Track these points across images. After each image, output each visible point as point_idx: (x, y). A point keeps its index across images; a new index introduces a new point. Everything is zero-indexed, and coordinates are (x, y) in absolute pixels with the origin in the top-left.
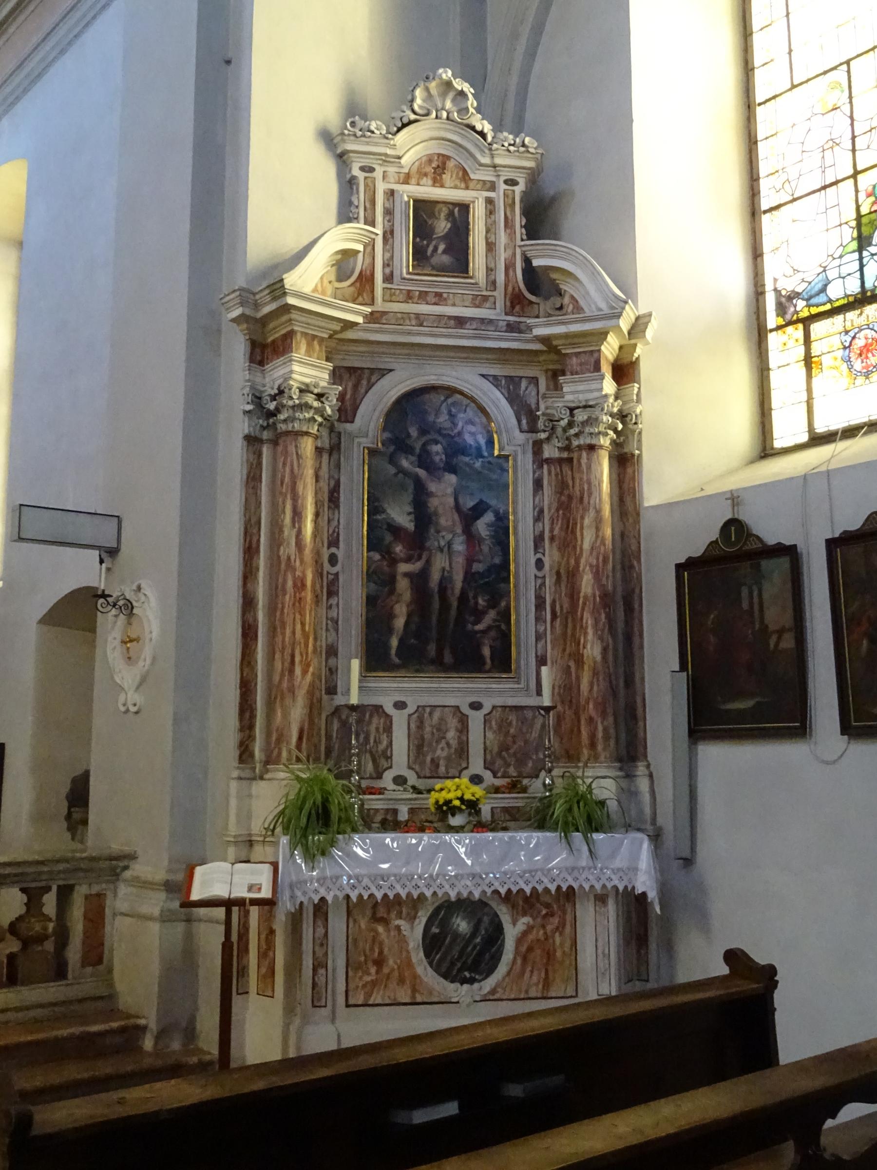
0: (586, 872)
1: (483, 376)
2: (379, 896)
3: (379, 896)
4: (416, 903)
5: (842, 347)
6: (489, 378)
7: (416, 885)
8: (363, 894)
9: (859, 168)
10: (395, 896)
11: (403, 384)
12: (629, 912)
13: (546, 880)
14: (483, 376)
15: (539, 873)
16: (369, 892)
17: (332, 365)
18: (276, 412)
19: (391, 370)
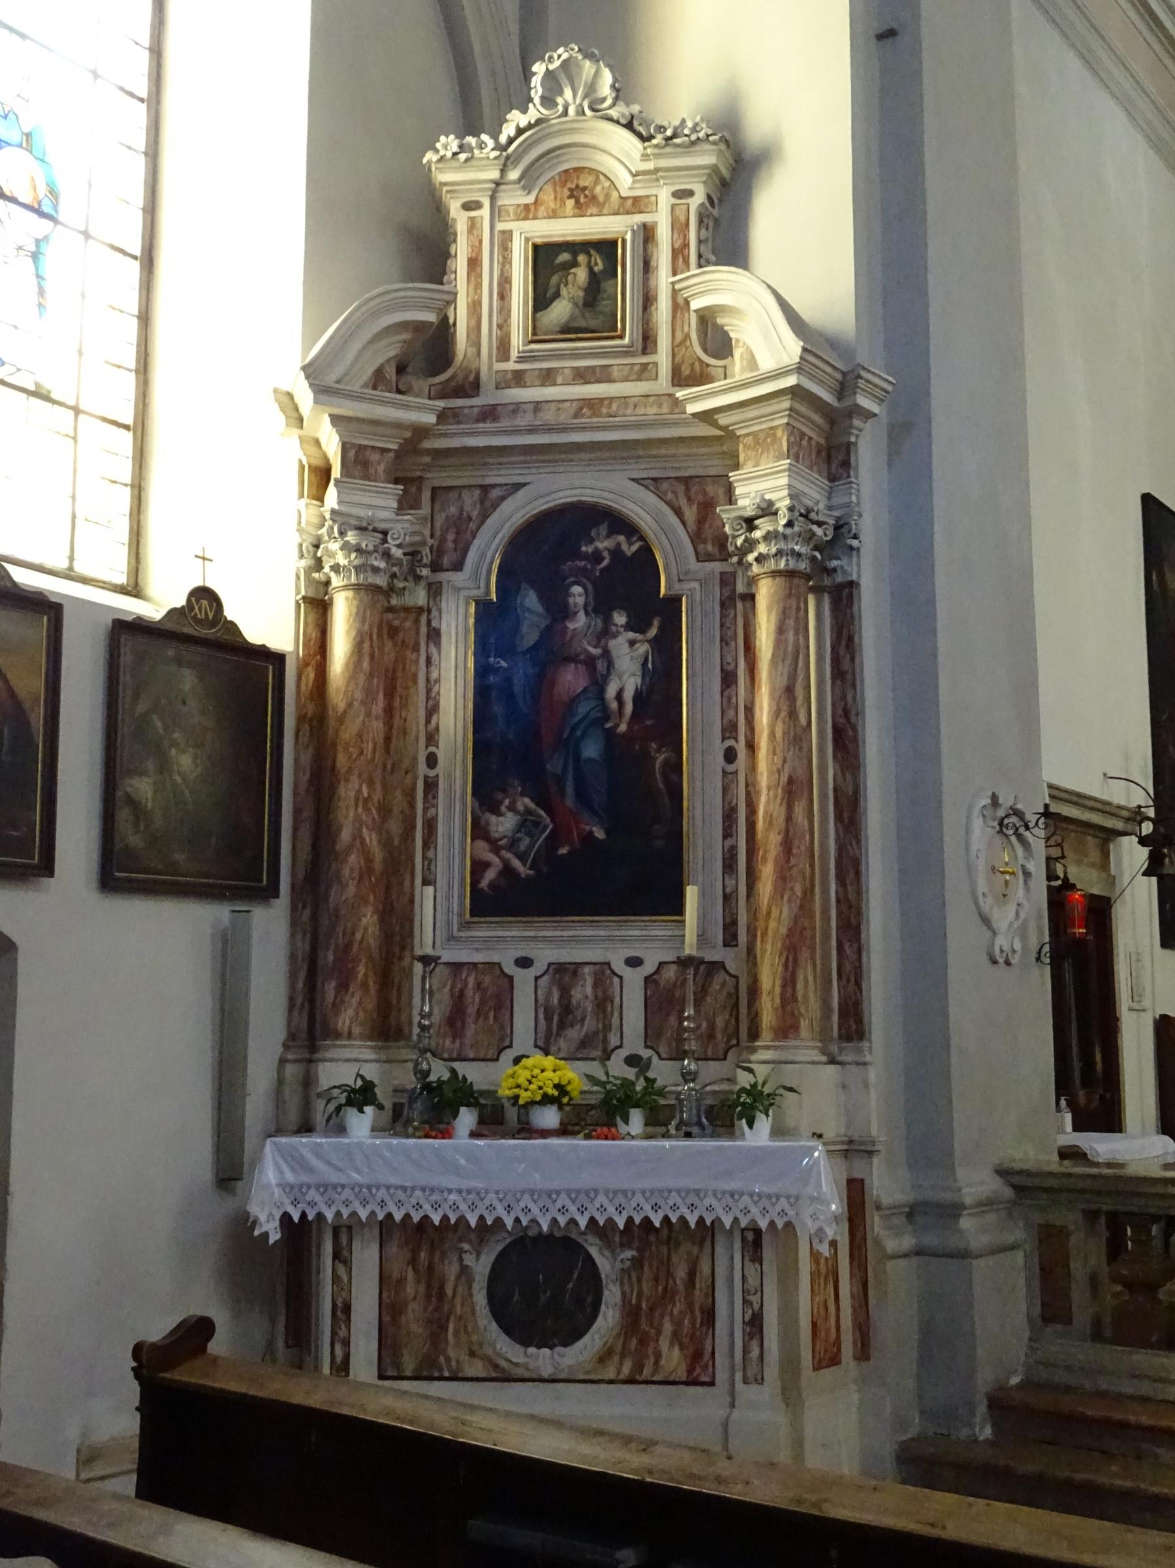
0: (383, 1191)
1: (633, 480)
2: (398, 1216)
3: (398, 1216)
4: (486, 1230)
5: (81, 417)
6: (645, 482)
7: (418, 1204)
8: (705, 1217)
9: (82, 229)
10: (678, 1219)
11: (544, 500)
12: (318, 1273)
13: (573, 1209)
14: (633, 480)
15: (563, 1195)
16: (786, 1219)
17: (402, 487)
18: (781, 536)
19: (524, 485)
